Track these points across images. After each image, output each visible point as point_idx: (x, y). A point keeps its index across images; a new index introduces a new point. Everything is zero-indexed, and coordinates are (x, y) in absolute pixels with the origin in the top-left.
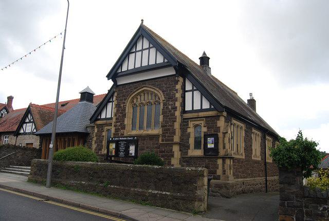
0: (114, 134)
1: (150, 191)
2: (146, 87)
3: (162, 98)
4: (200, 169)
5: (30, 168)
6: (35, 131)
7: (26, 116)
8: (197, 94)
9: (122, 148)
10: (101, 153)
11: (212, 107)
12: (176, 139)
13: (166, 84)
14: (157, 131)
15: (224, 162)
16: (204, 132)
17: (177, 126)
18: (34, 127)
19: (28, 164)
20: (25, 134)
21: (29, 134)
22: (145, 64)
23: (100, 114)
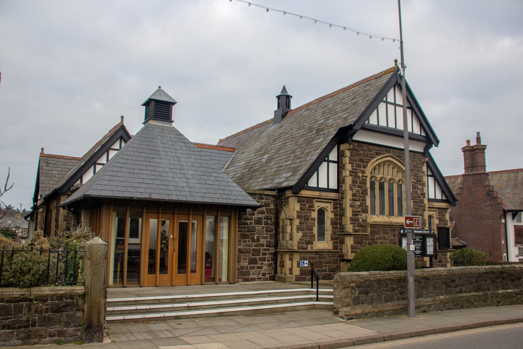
10: (312, 248)
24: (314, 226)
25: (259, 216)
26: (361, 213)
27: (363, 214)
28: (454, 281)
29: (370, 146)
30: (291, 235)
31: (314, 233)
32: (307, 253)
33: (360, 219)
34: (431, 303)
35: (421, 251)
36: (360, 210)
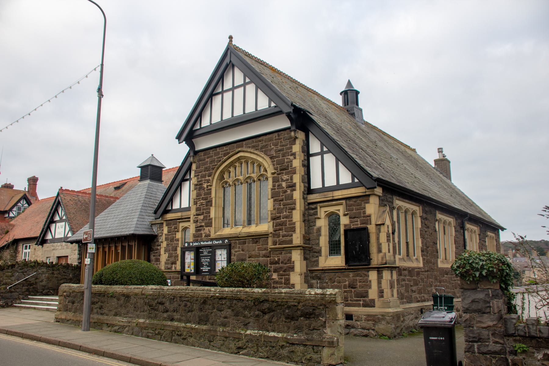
0: (194, 236)
1: (248, 332)
2: (243, 151)
3: (270, 170)
4: (329, 291)
5: (57, 298)
6: (70, 235)
7: (54, 210)
8: (330, 160)
9: (205, 261)
10: (175, 268)
11: (356, 180)
12: (297, 239)
13: (276, 145)
14: (265, 227)
15: (380, 277)
16: (345, 225)
17: (297, 216)
18: (68, 229)
19: (54, 291)
20: (54, 240)
21: (60, 240)
22: (238, 112)
23: (171, 201)
24: (178, 246)
27: (206, 228)
28: (162, 303)
29: (218, 149)
32: (171, 273)
33: (203, 234)
34: (125, 324)
35: (210, 268)
36: (203, 224)
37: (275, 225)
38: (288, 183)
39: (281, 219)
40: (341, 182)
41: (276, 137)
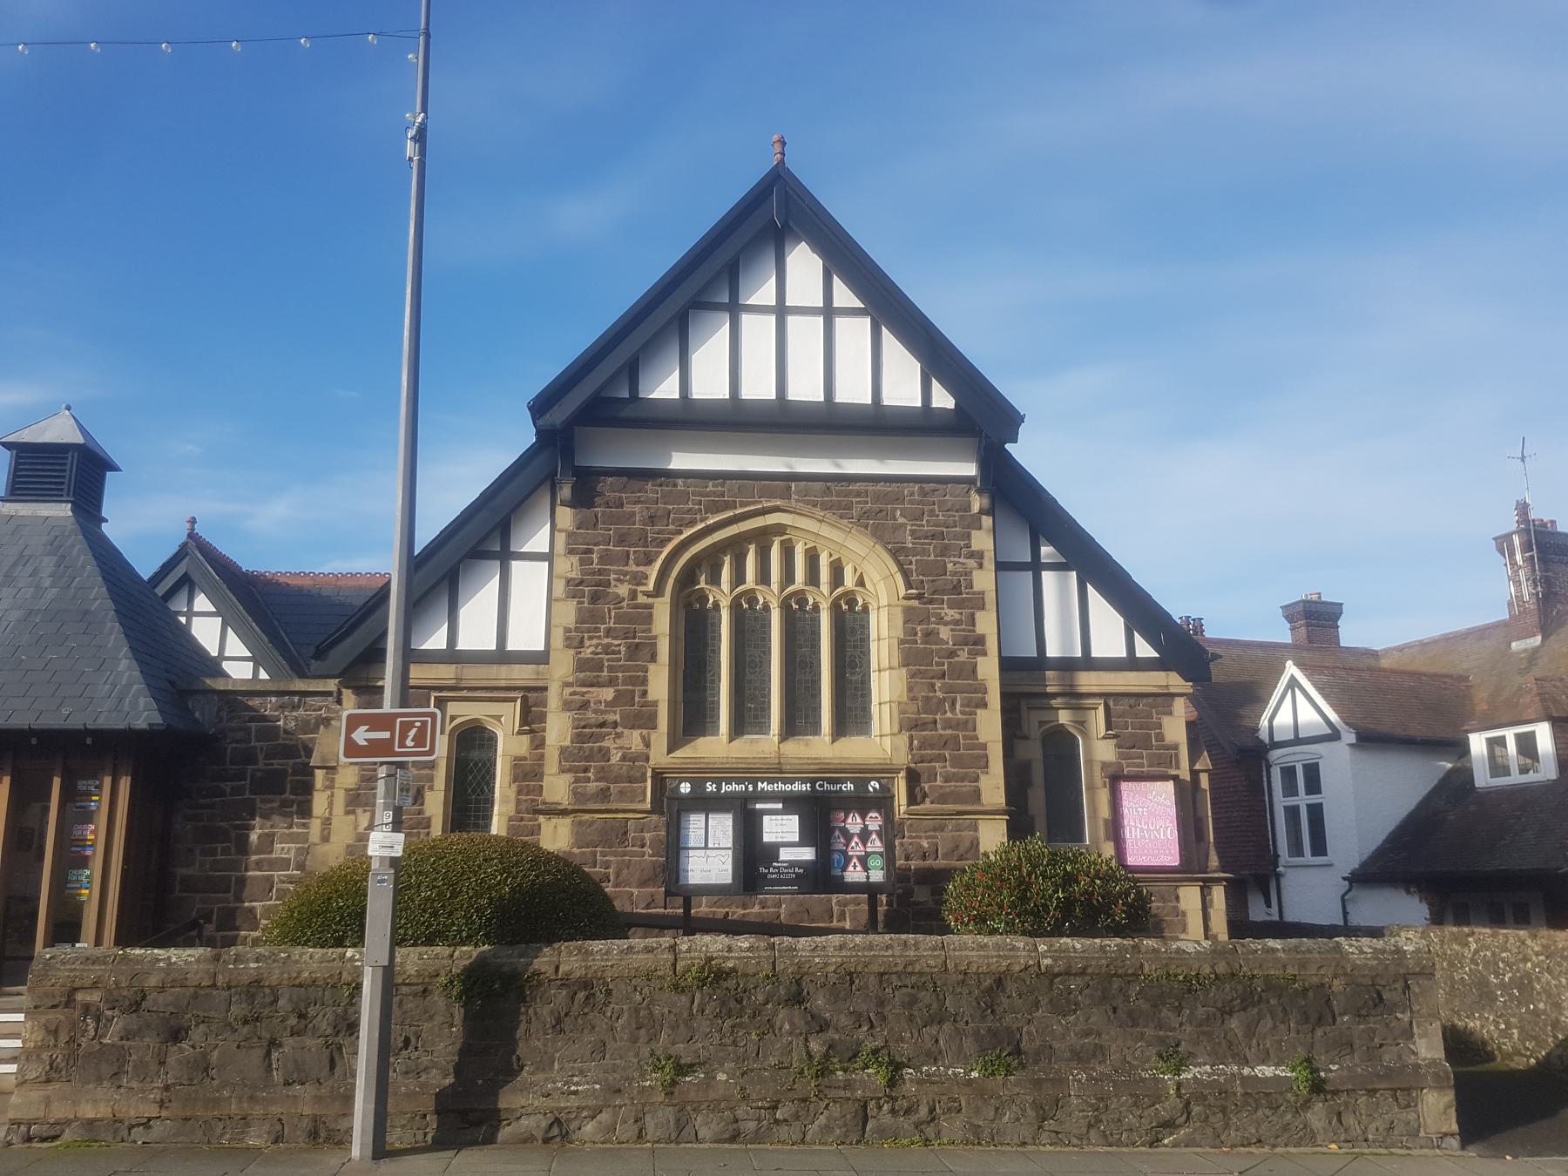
24: (431, 788)
25: (272, 764)
26: (619, 729)
27: (626, 732)
30: (327, 822)
31: (427, 814)
36: (611, 717)
37: (916, 742)
38: (960, 631)
39: (256, 726)
40: (511, 646)
41: (912, 494)
